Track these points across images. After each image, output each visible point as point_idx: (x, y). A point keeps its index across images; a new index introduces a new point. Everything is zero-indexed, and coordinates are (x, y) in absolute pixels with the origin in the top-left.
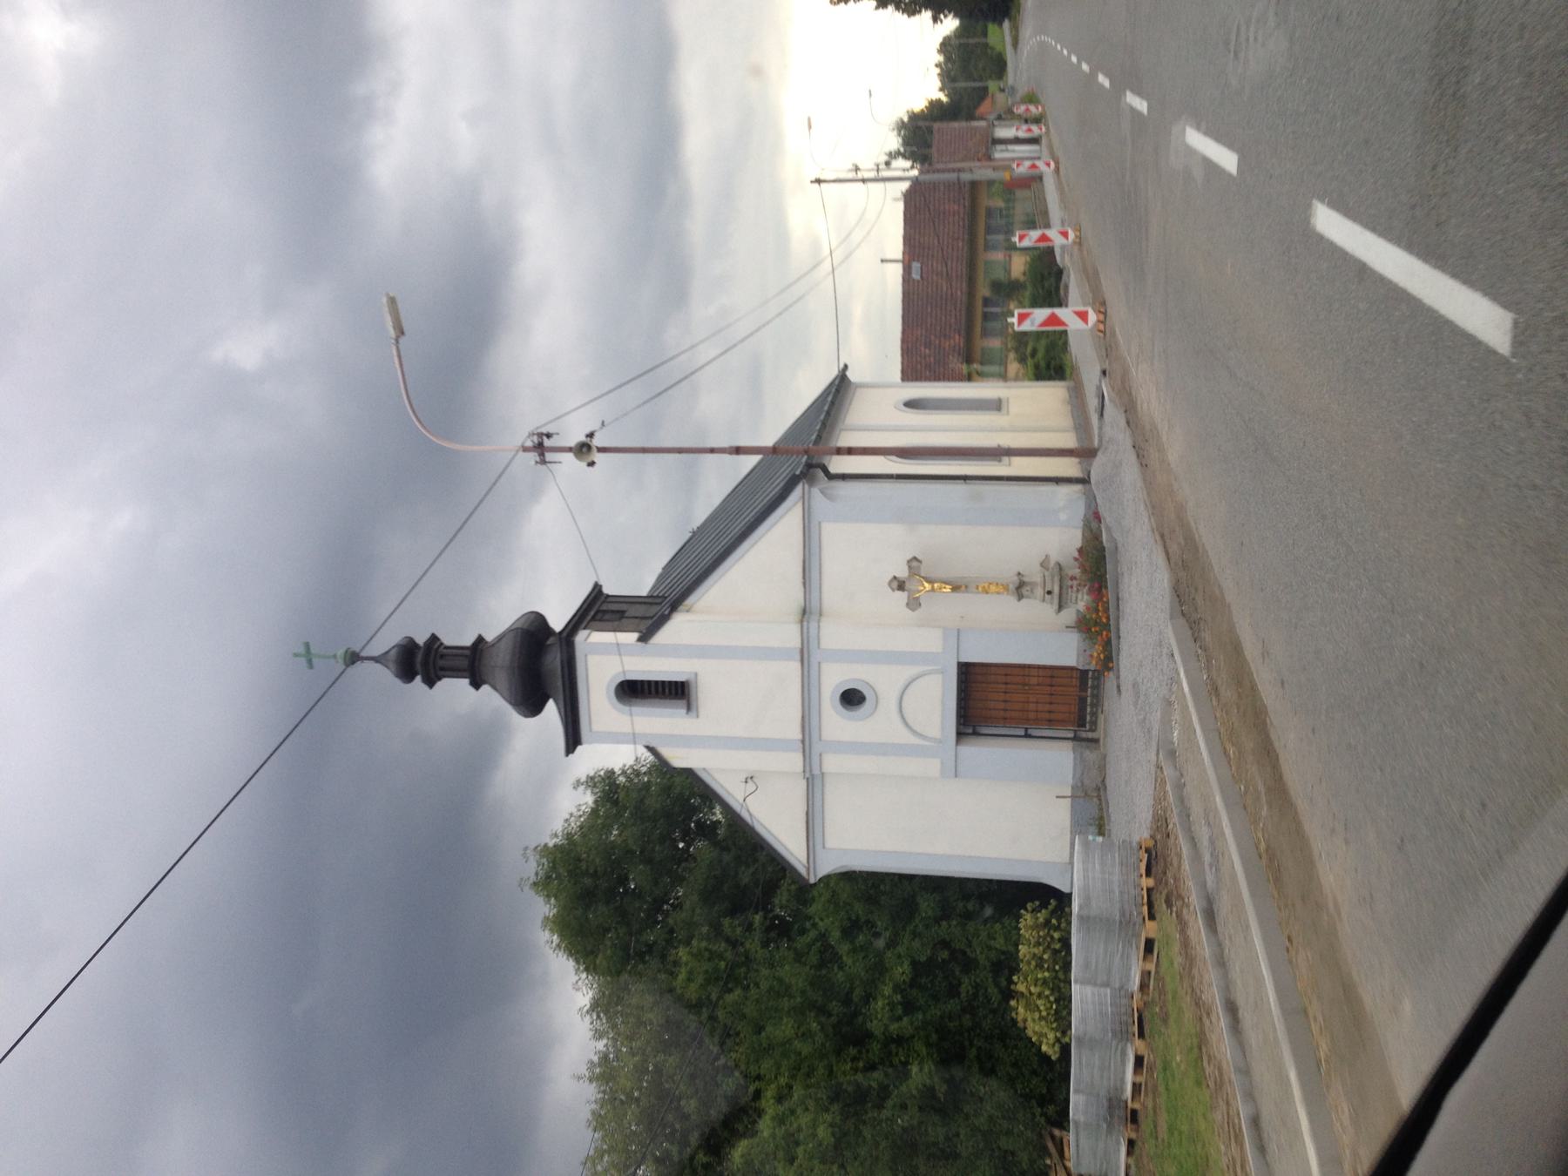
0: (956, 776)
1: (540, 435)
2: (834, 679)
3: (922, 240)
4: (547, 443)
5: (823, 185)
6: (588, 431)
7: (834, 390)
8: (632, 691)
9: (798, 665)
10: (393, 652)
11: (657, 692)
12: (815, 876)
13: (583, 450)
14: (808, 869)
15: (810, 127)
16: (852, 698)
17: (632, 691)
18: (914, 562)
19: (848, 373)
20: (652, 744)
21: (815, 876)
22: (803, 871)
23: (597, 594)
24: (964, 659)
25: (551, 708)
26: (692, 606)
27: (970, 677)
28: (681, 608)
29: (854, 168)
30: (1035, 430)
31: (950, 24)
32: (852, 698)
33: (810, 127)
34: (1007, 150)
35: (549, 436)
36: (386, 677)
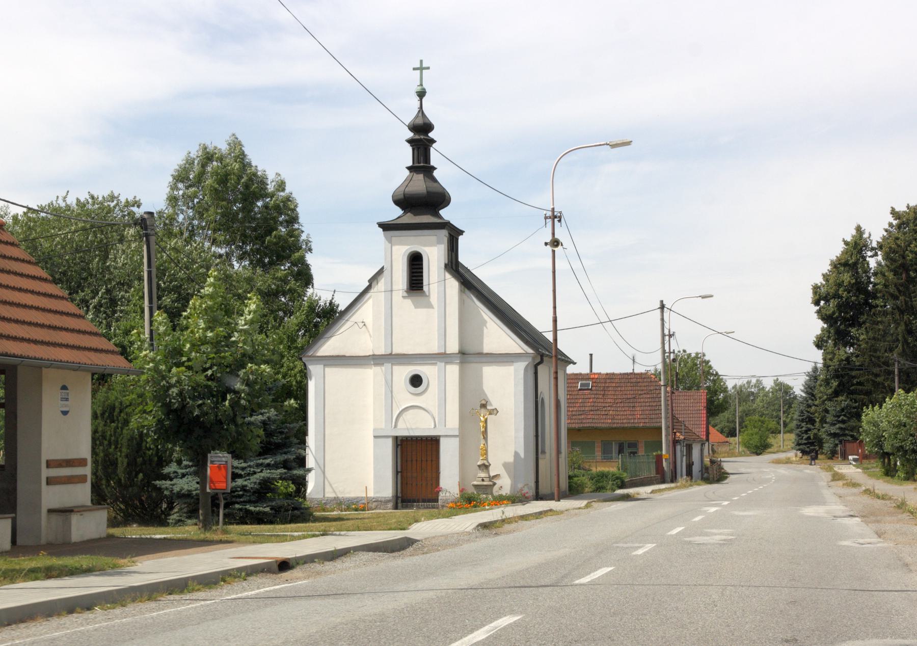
0: (375, 437)
1: (560, 217)
2: (426, 371)
3: (610, 389)
4: (556, 220)
5: (659, 311)
6: (563, 244)
7: (563, 358)
8: (415, 262)
9: (436, 352)
10: (428, 122)
11: (413, 273)
12: (306, 361)
13: (555, 243)
14: (310, 356)
15: (703, 297)
16: (416, 381)
17: (415, 262)
18: (495, 412)
19: (572, 365)
20: (386, 273)
21: (306, 361)
22: (310, 353)
23: (461, 232)
24: (443, 442)
25: (398, 211)
26: (464, 292)
27: (430, 445)
28: (463, 287)
29: (671, 333)
30: (732, 462)
31: (825, 326)
32: (416, 381)
33: (703, 297)
34: (682, 456)
35: (560, 221)
36: (410, 116)
